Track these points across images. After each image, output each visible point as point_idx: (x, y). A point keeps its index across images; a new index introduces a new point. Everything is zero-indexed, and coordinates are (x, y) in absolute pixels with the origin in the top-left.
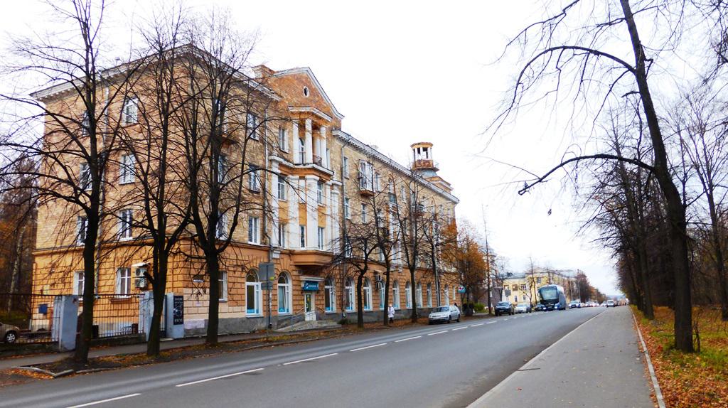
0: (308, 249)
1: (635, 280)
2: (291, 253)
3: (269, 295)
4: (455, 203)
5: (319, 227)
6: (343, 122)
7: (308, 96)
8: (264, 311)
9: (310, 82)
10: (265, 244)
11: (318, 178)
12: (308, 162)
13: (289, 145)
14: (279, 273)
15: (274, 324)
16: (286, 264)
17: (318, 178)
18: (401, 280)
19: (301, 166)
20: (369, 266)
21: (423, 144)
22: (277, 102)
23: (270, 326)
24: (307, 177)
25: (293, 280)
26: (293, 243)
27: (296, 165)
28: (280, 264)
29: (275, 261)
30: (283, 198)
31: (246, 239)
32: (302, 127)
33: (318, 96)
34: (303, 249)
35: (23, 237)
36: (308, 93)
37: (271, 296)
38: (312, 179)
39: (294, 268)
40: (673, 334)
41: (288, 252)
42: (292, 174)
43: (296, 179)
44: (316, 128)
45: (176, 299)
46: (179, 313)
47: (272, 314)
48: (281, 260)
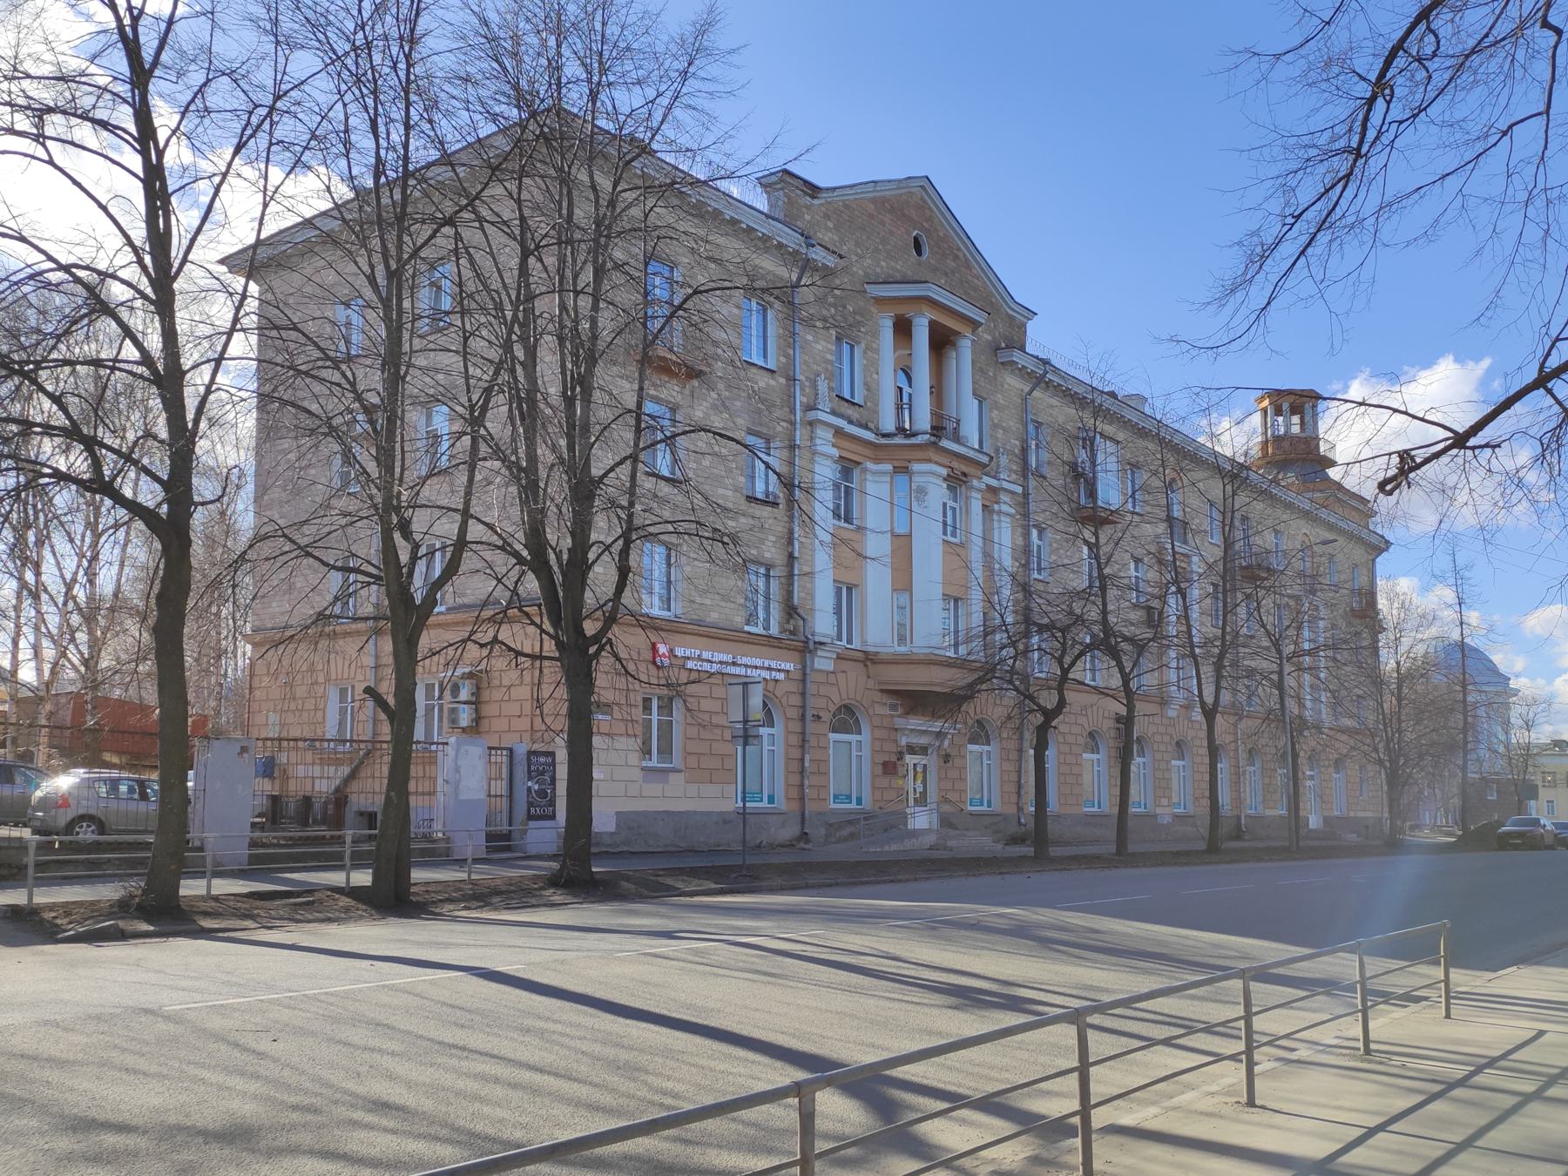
0: (914, 650)
1: (937, 652)
2: (869, 659)
3: (802, 760)
4: (1380, 551)
5: (946, 597)
6: (1032, 327)
7: (925, 257)
8: (788, 799)
9: (930, 219)
10: (793, 633)
11: (944, 472)
12: (917, 427)
13: (866, 384)
14: (833, 708)
15: (817, 832)
16: (853, 686)
17: (944, 472)
18: (1158, 739)
19: (899, 440)
20: (1070, 696)
21: (1291, 392)
22: (827, 272)
23: (804, 836)
24: (916, 467)
25: (874, 727)
26: (877, 631)
27: (885, 436)
28: (1086, 715)
29: (822, 678)
30: (848, 520)
31: (739, 620)
32: (903, 329)
33: (956, 257)
34: (902, 649)
35: (1291, 723)
36: (926, 250)
37: (807, 764)
38: (931, 477)
39: (878, 696)
40: (414, 747)
41: (860, 655)
42: (877, 460)
43: (885, 473)
44: (941, 342)
45: (534, 759)
46: (542, 793)
47: (811, 807)
48: (841, 677)
